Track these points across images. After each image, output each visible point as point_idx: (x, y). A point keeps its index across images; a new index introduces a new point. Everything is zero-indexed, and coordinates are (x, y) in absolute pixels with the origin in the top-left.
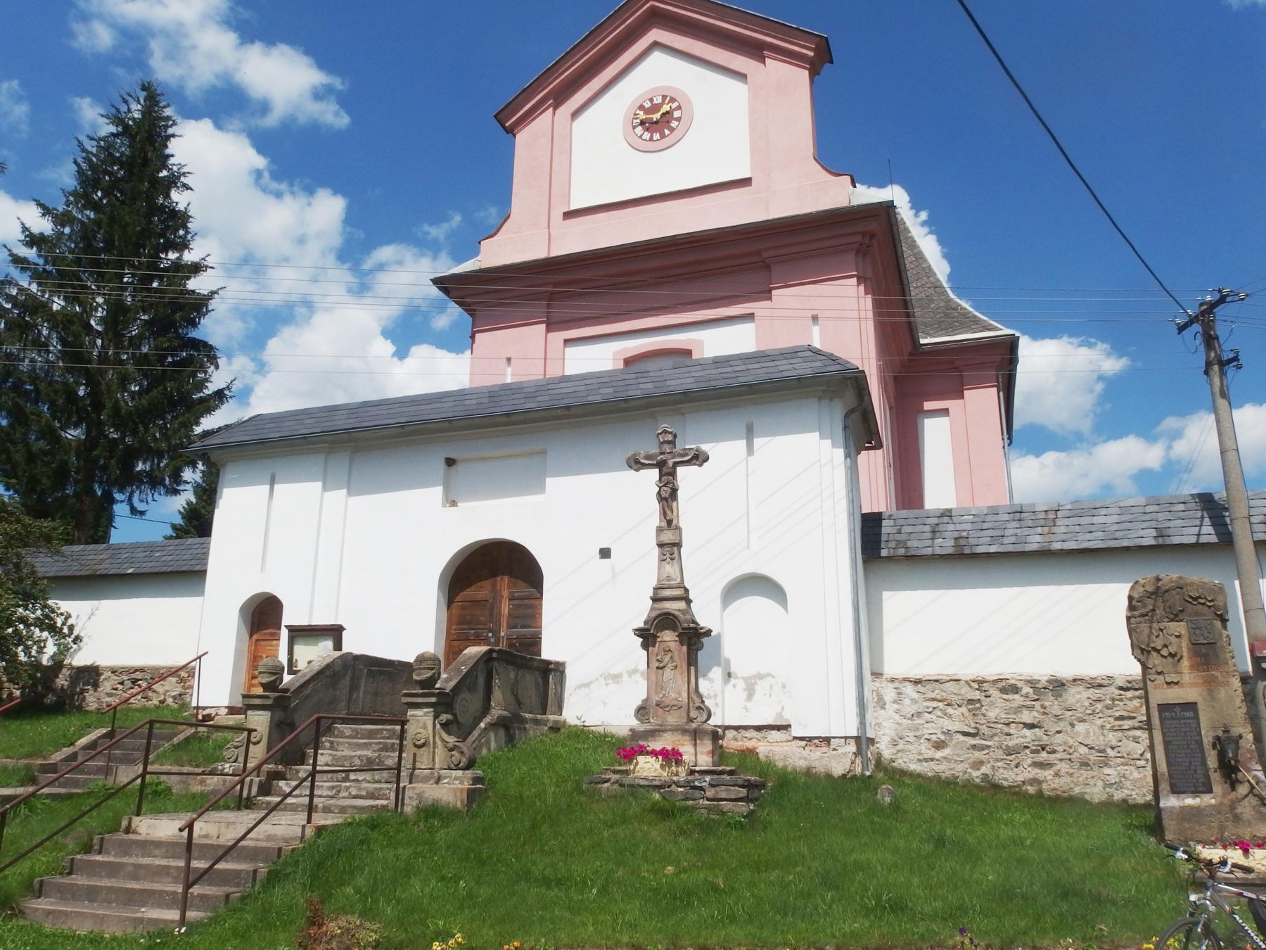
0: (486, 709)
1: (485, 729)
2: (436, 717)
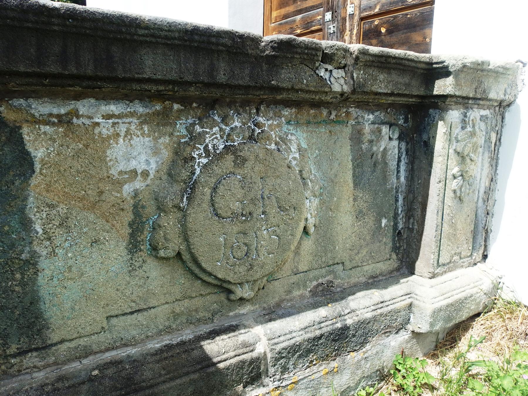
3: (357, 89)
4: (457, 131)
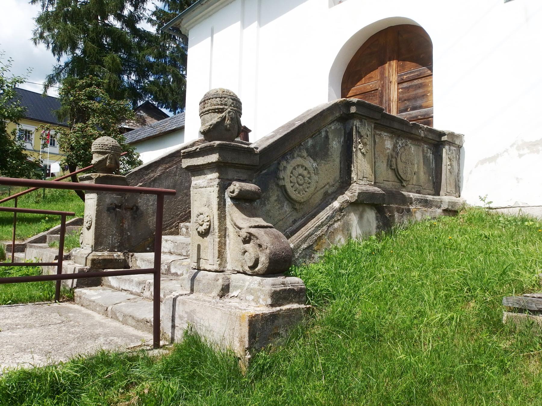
0: (345, 182)
1: (341, 210)
2: (223, 187)
3: (425, 137)
4: (448, 152)
